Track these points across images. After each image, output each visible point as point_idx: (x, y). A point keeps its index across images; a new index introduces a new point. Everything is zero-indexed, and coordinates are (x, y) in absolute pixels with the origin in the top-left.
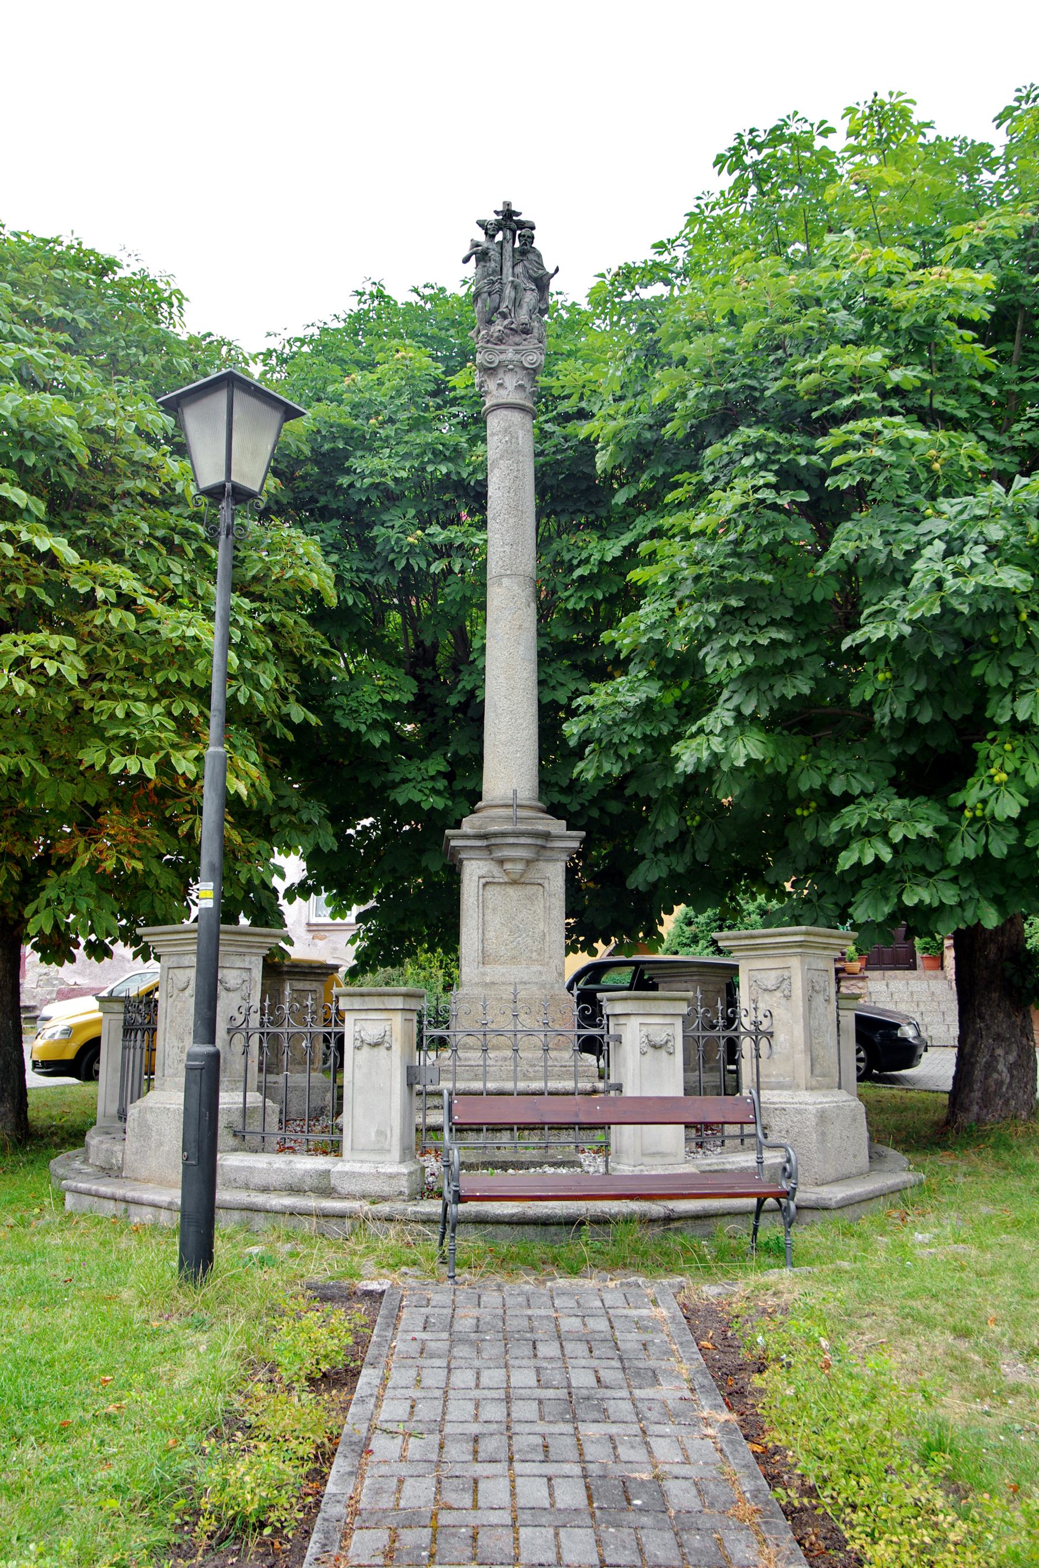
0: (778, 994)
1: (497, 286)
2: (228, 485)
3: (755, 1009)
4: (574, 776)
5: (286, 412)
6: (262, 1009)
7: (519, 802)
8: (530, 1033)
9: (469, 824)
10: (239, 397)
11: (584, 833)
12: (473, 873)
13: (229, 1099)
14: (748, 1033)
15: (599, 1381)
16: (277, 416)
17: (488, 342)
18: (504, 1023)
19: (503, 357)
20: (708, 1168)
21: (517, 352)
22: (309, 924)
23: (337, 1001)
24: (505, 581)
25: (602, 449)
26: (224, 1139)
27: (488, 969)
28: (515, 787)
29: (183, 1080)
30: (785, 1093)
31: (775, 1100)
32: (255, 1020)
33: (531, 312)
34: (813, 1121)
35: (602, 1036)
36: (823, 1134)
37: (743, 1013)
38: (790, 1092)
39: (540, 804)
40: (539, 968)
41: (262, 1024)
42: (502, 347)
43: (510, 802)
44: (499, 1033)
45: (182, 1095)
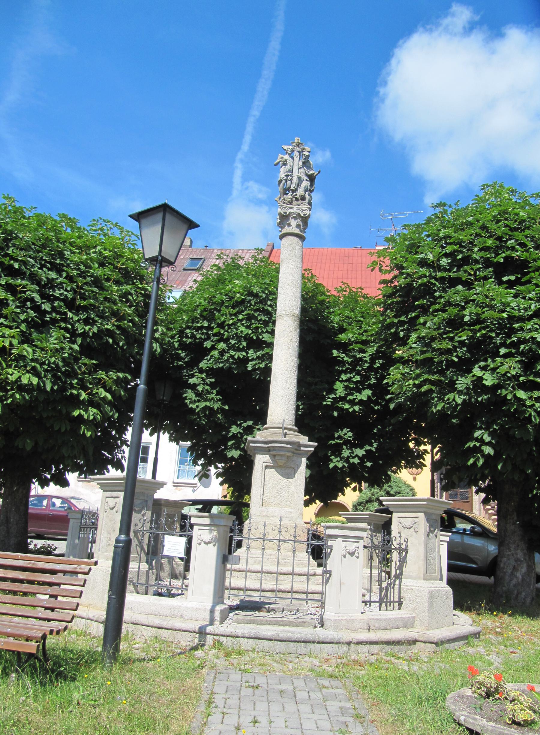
0: (412, 530)
1: (289, 178)
2: (160, 258)
3: (400, 537)
4: (89, 551)
5: (190, 225)
6: (152, 520)
7: (285, 426)
8: (287, 541)
9: (260, 435)
10: (168, 217)
11: (316, 444)
12: (260, 460)
13: (133, 566)
14: (396, 549)
15: (317, 727)
16: (185, 227)
17: (284, 203)
18: (273, 534)
19: (291, 211)
20: (373, 617)
21: (298, 209)
22: (174, 483)
23: (190, 519)
24: (286, 318)
25: (243, 315)
26: (130, 587)
27: (264, 508)
28: (284, 418)
29: (112, 554)
30: (413, 581)
31: (408, 584)
32: (148, 526)
33: (306, 191)
34: (426, 597)
35: (323, 545)
36: (431, 603)
37: (394, 539)
38: (415, 581)
39: (296, 428)
40: (291, 510)
41: (151, 528)
42: (291, 206)
43: (281, 426)
44: (271, 540)
45: (111, 562)
